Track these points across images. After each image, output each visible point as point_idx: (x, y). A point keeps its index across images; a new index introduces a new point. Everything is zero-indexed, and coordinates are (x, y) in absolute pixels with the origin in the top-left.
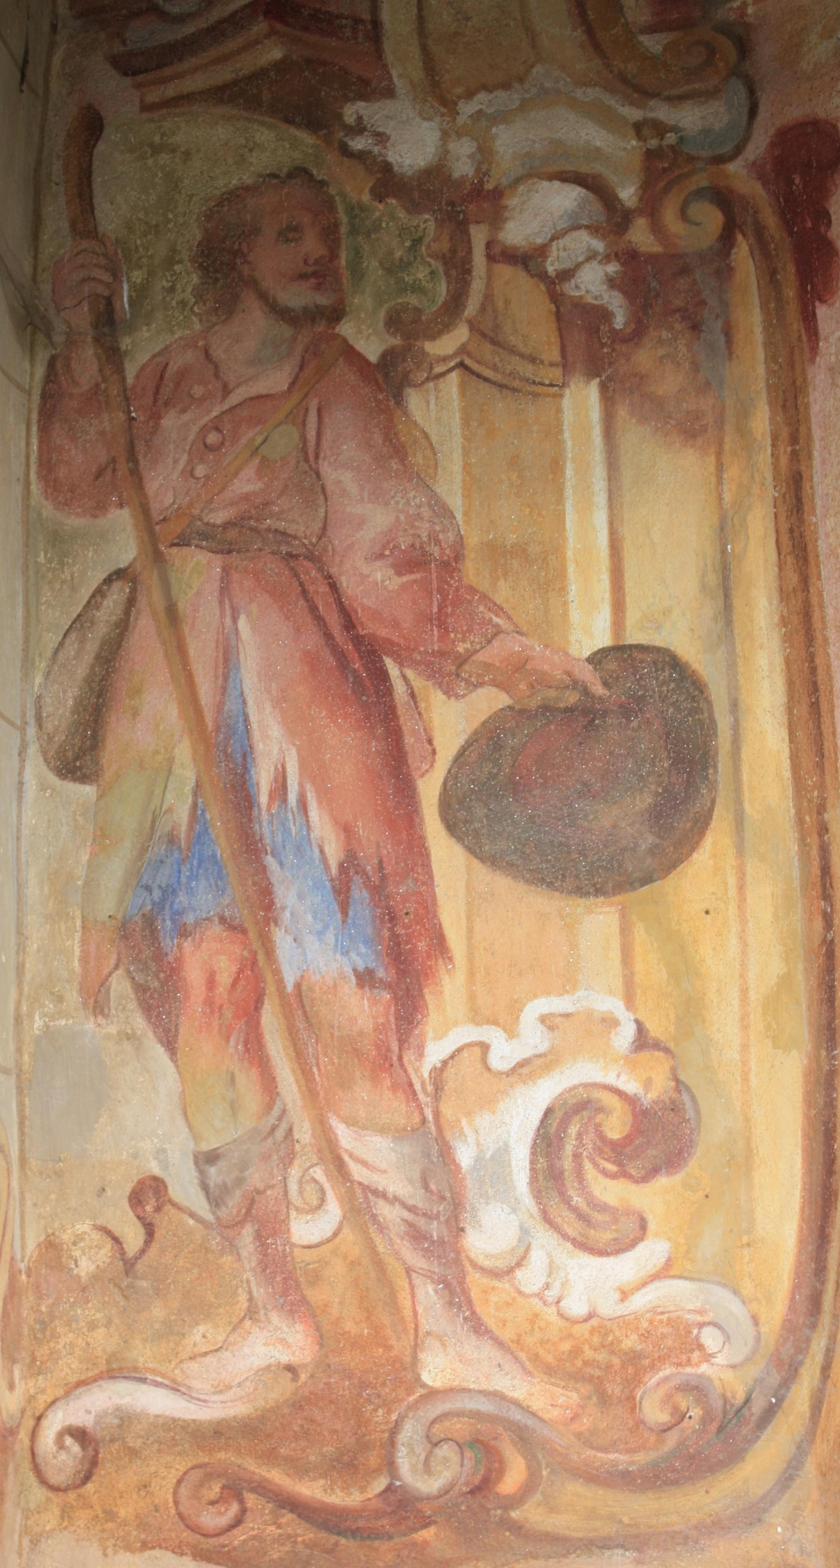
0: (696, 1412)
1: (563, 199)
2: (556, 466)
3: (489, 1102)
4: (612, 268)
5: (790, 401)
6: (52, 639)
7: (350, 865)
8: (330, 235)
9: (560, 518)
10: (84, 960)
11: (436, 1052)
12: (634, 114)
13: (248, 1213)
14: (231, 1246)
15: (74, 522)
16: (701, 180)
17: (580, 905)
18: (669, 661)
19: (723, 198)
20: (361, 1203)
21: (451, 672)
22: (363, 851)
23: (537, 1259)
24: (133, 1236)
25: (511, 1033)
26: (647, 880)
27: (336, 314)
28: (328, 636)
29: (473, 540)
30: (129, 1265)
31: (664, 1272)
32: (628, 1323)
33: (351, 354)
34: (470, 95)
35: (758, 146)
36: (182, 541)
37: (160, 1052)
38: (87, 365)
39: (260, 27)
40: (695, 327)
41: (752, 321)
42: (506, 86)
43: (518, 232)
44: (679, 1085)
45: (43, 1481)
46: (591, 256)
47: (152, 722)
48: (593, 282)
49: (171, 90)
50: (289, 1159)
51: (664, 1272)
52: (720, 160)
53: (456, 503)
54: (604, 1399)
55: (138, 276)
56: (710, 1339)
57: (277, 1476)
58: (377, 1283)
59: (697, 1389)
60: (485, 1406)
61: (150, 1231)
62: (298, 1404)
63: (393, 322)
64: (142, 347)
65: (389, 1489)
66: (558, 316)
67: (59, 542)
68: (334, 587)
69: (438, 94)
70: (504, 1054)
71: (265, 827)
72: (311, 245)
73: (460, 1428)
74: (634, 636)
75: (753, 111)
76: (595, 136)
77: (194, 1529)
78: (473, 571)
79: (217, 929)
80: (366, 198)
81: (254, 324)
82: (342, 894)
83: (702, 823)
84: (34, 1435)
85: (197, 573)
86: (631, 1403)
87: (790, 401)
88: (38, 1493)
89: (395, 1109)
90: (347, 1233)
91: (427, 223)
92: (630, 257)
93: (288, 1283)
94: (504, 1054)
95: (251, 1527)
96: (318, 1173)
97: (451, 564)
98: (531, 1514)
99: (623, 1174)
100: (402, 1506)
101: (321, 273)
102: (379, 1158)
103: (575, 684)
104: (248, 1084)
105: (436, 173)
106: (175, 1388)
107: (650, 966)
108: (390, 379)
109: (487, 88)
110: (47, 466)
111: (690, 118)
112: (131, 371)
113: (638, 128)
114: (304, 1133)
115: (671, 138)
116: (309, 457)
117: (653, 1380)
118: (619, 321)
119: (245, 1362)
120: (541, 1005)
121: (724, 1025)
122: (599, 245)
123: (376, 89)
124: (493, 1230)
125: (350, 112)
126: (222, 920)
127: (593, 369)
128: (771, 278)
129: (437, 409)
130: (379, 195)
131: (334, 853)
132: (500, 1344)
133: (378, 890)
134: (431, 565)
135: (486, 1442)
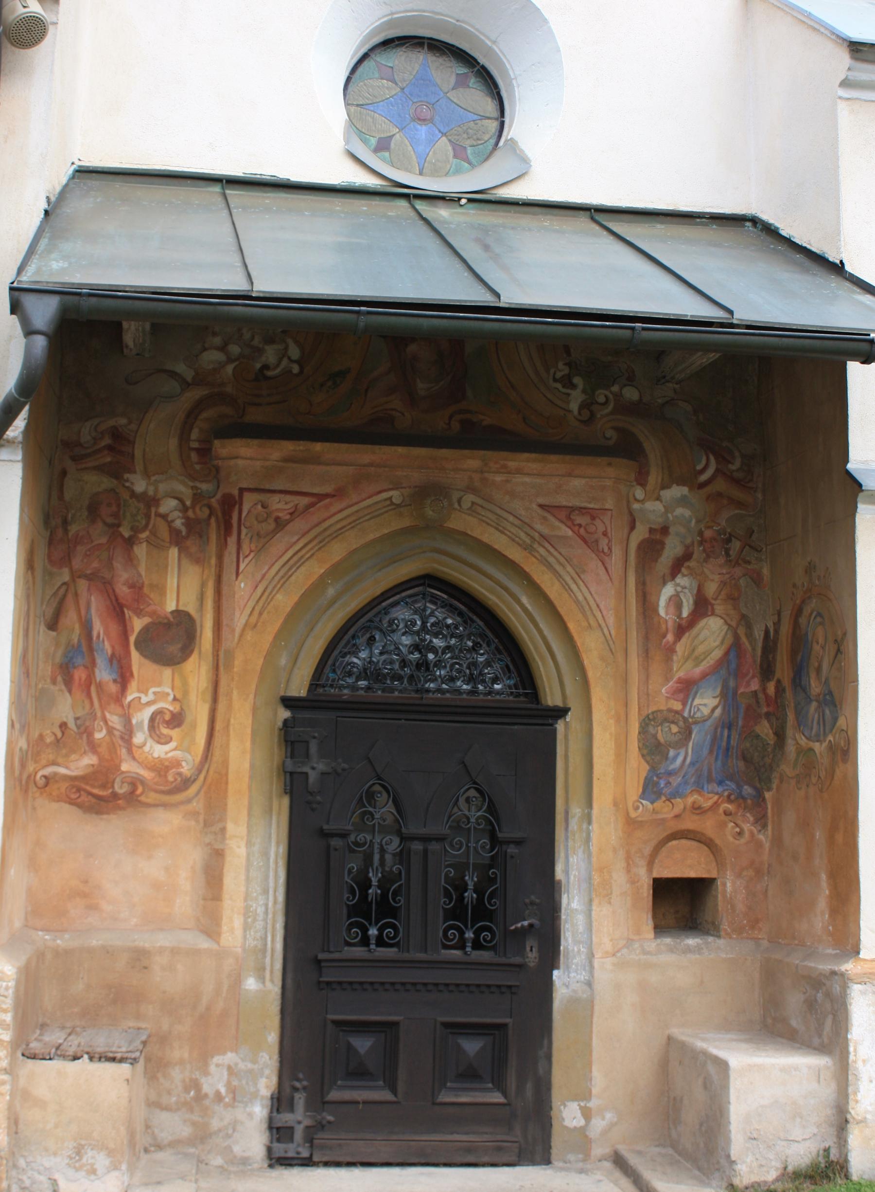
0: (179, 779)
1: (173, 503)
2: (166, 567)
3: (140, 710)
4: (183, 521)
5: (220, 557)
6: (48, 597)
7: (113, 655)
8: (119, 506)
9: (166, 580)
10: (52, 672)
11: (129, 698)
12: (191, 484)
13: (85, 731)
14: (81, 738)
15: (55, 570)
16: (205, 502)
17: (163, 668)
18: (187, 614)
19: (210, 507)
20: (110, 730)
21: (139, 613)
22: (237, 981)
23: (148, 745)
24: (59, 735)
25: (146, 695)
26: (179, 663)
27: (119, 525)
28: (111, 602)
29: (146, 583)
30: (58, 741)
31: (175, 749)
32: (167, 759)
33: (122, 536)
34: (154, 475)
35: (219, 496)
36: (79, 577)
37: (67, 694)
38: (60, 532)
39: (106, 452)
40: (201, 536)
41: (213, 536)
42: (162, 474)
43: (163, 509)
44: (182, 709)
45: (36, 786)
46: (179, 517)
47: (70, 619)
48: (178, 523)
49: (84, 466)
50: (95, 720)
51: (175, 749)
52: (210, 498)
53: (143, 573)
54: (160, 776)
55: (73, 511)
56: (184, 764)
57: (88, 788)
58: (112, 748)
59: (180, 774)
60: (134, 775)
61: (63, 733)
62: (94, 773)
63: (132, 529)
64: (73, 529)
65: (112, 792)
66: (170, 531)
67: (51, 574)
68: (114, 591)
69: (147, 474)
70: (144, 699)
71: (95, 645)
72: (114, 508)
73: (129, 780)
74: (181, 608)
75: (218, 487)
76: (181, 488)
77: (69, 798)
78: (146, 590)
79: (82, 668)
80: (128, 498)
81: (100, 525)
82: (111, 661)
83: (192, 652)
84: (35, 776)
85: (82, 584)
86: (166, 776)
87: (220, 557)
88: (35, 789)
89: (119, 710)
90: (107, 737)
91: (142, 506)
92: (187, 519)
93: (93, 747)
94: (144, 699)
95: (82, 798)
96: (101, 723)
97: (141, 588)
98: (143, 799)
99: (168, 727)
100: (115, 796)
101: (116, 515)
102: (115, 720)
103: (167, 618)
104: (87, 702)
105: (145, 494)
106: (67, 768)
107: (178, 682)
108: (130, 542)
109: (158, 474)
110: (49, 556)
111: (204, 487)
112: (70, 534)
113: (192, 488)
114: (99, 714)
115: (199, 491)
116: (110, 559)
117: (171, 772)
118: (184, 533)
119: (83, 763)
120: (152, 690)
121: (193, 697)
122: (181, 515)
123: (132, 471)
124: (139, 738)
125: (126, 476)
126: (84, 666)
127: (177, 544)
128: (218, 527)
129: (141, 551)
130: (131, 498)
131: (110, 652)
132: (138, 762)
133: (119, 661)
134: (137, 587)
135: (134, 782)
